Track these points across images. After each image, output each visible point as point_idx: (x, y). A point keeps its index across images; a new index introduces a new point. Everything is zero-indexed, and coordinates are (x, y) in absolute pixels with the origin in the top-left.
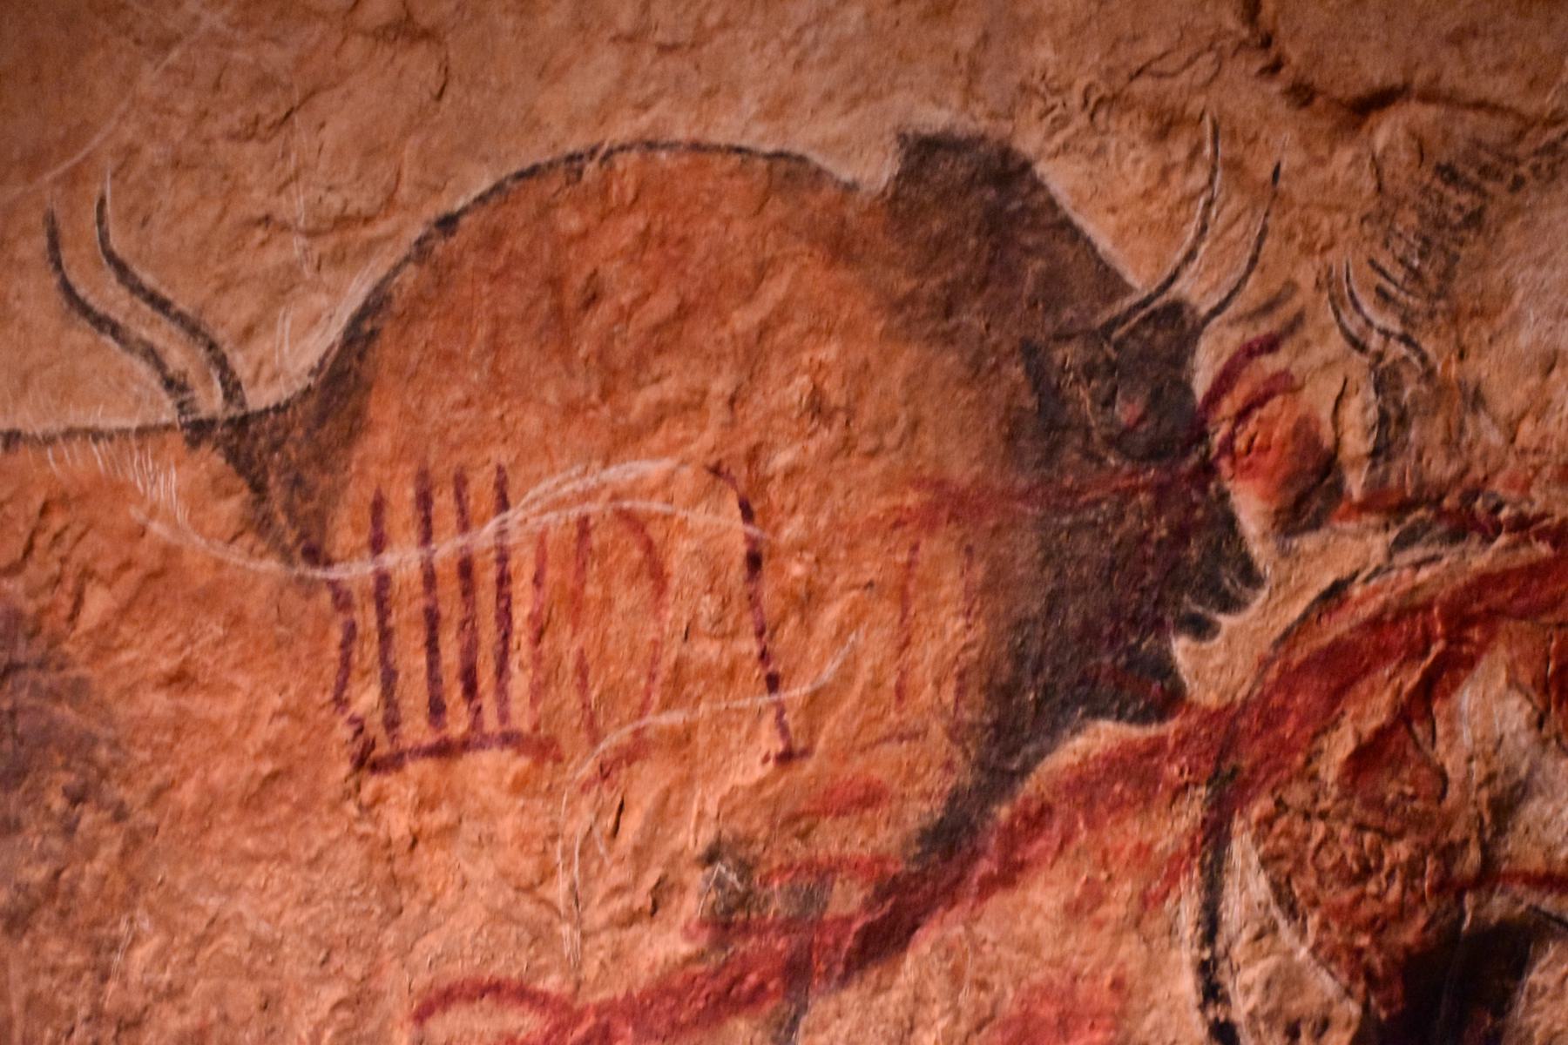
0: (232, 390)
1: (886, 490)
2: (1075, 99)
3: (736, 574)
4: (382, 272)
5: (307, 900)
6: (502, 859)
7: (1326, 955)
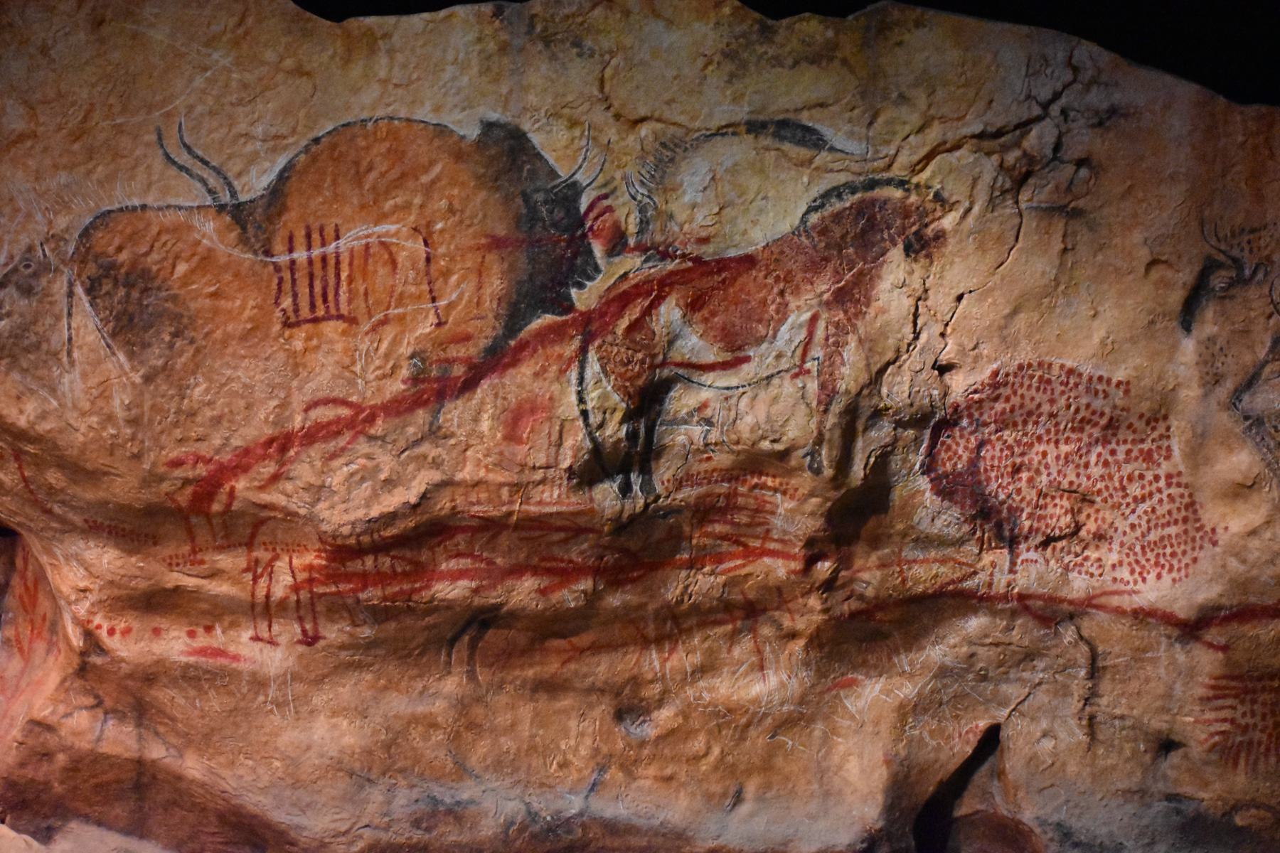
0: (233, 194)
1: (474, 238)
2: (543, 114)
3: (422, 264)
4: (291, 156)
5: (265, 371)
6: (336, 358)
7: (617, 388)
